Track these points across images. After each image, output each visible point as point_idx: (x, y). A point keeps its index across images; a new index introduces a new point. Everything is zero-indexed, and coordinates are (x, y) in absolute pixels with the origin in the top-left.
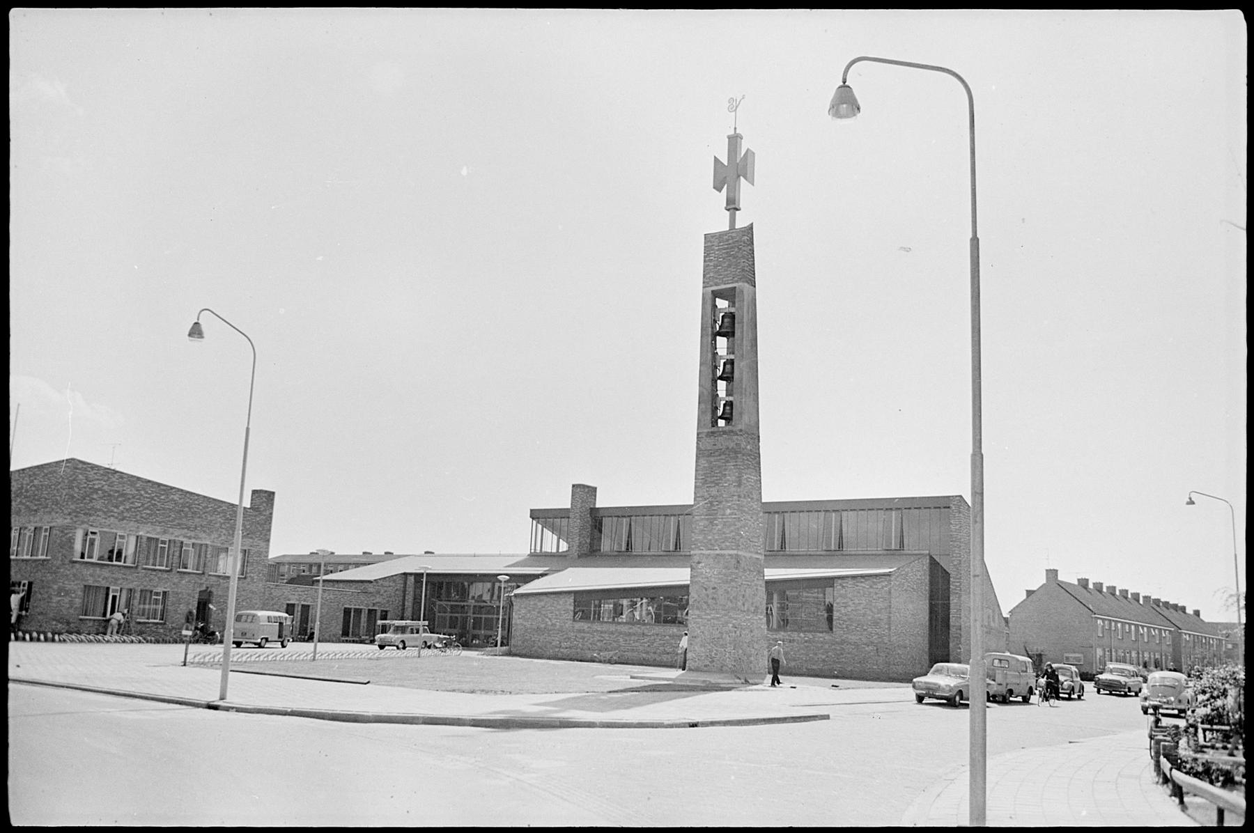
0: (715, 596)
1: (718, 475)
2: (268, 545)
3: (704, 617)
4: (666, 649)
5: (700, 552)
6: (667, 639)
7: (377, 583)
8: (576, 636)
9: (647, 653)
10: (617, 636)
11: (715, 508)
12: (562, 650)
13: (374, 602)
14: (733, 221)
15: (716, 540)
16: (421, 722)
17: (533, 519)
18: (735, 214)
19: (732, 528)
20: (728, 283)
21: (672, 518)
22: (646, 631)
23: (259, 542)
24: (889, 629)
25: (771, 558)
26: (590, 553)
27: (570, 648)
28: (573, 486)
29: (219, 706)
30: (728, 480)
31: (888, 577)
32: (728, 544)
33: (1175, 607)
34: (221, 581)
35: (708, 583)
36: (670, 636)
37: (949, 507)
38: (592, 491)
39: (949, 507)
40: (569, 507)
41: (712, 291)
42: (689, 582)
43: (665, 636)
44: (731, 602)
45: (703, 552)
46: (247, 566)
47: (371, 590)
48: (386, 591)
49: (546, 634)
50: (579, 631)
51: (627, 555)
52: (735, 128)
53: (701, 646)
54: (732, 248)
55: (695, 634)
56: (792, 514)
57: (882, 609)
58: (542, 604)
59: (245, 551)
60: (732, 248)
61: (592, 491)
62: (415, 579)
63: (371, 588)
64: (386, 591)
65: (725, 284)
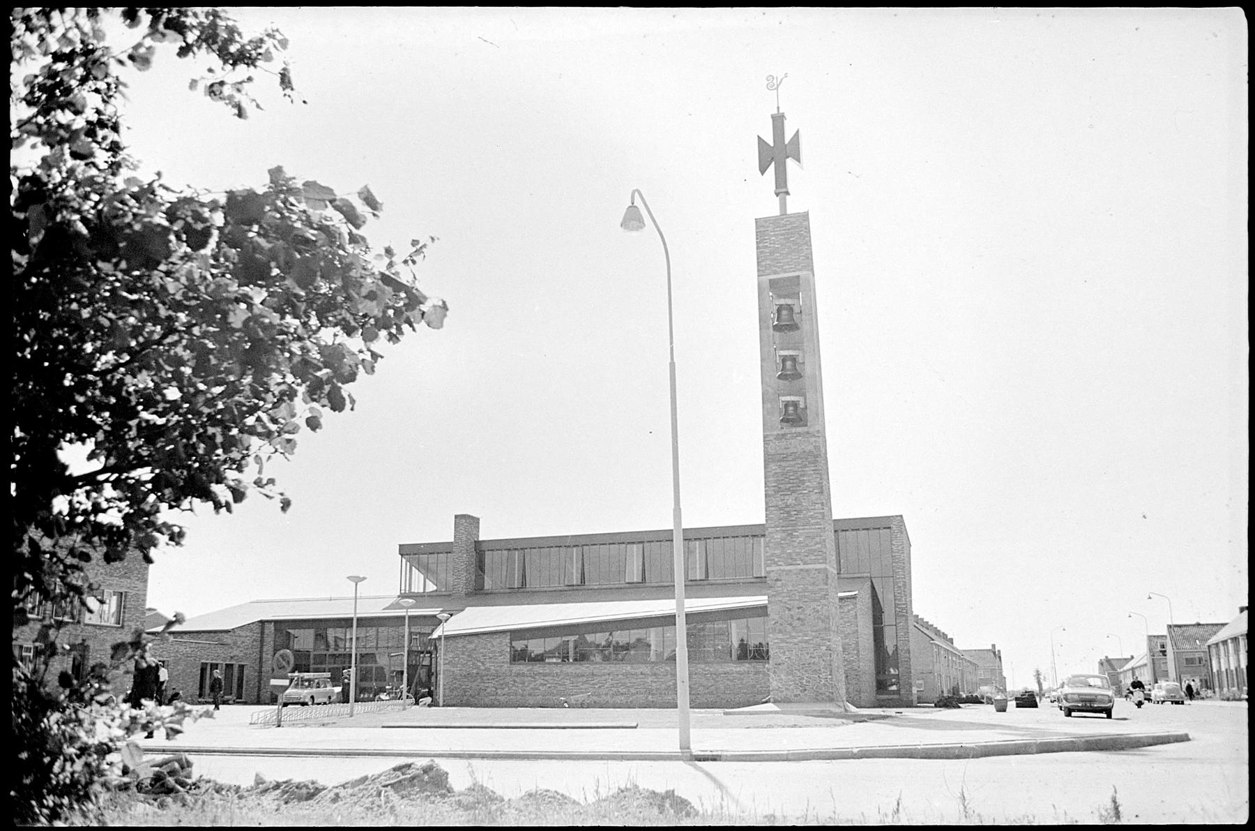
0: (802, 616)
1: (795, 481)
2: (146, 586)
3: (788, 641)
4: (620, 690)
5: (778, 568)
6: (621, 679)
7: (234, 632)
8: (515, 681)
9: (599, 695)
10: (563, 678)
11: (793, 519)
12: (498, 698)
13: (232, 655)
14: (783, 205)
15: (798, 554)
16: (1035, 750)
17: (402, 555)
18: (785, 200)
19: (818, 539)
20: (789, 272)
21: (575, 549)
22: (595, 671)
23: (136, 582)
24: (858, 654)
25: (632, 590)
26: (478, 593)
27: (508, 694)
28: (456, 517)
29: (720, 756)
30: (807, 486)
31: (853, 600)
32: (813, 558)
33: (944, 636)
34: (98, 631)
35: (791, 602)
36: (623, 675)
37: (889, 528)
38: (474, 522)
39: (889, 528)
40: (452, 540)
41: (770, 280)
42: (767, 602)
43: (618, 675)
44: (823, 621)
45: (782, 568)
46: (124, 612)
47: (229, 641)
48: (243, 642)
49: (479, 680)
50: (518, 675)
51: (520, 592)
52: (778, 108)
53: (788, 674)
54: (792, 233)
55: (780, 661)
56: (716, 540)
57: (849, 634)
58: (472, 646)
59: (122, 593)
60: (792, 233)
61: (474, 522)
62: (275, 626)
63: (227, 639)
64: (243, 642)
65: (785, 272)
